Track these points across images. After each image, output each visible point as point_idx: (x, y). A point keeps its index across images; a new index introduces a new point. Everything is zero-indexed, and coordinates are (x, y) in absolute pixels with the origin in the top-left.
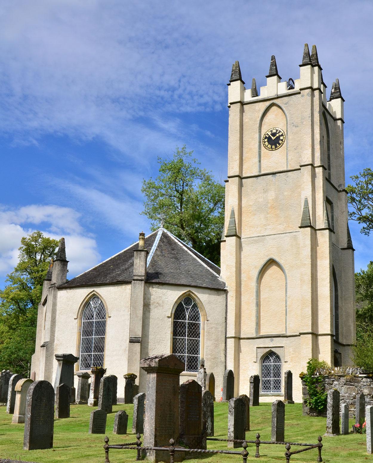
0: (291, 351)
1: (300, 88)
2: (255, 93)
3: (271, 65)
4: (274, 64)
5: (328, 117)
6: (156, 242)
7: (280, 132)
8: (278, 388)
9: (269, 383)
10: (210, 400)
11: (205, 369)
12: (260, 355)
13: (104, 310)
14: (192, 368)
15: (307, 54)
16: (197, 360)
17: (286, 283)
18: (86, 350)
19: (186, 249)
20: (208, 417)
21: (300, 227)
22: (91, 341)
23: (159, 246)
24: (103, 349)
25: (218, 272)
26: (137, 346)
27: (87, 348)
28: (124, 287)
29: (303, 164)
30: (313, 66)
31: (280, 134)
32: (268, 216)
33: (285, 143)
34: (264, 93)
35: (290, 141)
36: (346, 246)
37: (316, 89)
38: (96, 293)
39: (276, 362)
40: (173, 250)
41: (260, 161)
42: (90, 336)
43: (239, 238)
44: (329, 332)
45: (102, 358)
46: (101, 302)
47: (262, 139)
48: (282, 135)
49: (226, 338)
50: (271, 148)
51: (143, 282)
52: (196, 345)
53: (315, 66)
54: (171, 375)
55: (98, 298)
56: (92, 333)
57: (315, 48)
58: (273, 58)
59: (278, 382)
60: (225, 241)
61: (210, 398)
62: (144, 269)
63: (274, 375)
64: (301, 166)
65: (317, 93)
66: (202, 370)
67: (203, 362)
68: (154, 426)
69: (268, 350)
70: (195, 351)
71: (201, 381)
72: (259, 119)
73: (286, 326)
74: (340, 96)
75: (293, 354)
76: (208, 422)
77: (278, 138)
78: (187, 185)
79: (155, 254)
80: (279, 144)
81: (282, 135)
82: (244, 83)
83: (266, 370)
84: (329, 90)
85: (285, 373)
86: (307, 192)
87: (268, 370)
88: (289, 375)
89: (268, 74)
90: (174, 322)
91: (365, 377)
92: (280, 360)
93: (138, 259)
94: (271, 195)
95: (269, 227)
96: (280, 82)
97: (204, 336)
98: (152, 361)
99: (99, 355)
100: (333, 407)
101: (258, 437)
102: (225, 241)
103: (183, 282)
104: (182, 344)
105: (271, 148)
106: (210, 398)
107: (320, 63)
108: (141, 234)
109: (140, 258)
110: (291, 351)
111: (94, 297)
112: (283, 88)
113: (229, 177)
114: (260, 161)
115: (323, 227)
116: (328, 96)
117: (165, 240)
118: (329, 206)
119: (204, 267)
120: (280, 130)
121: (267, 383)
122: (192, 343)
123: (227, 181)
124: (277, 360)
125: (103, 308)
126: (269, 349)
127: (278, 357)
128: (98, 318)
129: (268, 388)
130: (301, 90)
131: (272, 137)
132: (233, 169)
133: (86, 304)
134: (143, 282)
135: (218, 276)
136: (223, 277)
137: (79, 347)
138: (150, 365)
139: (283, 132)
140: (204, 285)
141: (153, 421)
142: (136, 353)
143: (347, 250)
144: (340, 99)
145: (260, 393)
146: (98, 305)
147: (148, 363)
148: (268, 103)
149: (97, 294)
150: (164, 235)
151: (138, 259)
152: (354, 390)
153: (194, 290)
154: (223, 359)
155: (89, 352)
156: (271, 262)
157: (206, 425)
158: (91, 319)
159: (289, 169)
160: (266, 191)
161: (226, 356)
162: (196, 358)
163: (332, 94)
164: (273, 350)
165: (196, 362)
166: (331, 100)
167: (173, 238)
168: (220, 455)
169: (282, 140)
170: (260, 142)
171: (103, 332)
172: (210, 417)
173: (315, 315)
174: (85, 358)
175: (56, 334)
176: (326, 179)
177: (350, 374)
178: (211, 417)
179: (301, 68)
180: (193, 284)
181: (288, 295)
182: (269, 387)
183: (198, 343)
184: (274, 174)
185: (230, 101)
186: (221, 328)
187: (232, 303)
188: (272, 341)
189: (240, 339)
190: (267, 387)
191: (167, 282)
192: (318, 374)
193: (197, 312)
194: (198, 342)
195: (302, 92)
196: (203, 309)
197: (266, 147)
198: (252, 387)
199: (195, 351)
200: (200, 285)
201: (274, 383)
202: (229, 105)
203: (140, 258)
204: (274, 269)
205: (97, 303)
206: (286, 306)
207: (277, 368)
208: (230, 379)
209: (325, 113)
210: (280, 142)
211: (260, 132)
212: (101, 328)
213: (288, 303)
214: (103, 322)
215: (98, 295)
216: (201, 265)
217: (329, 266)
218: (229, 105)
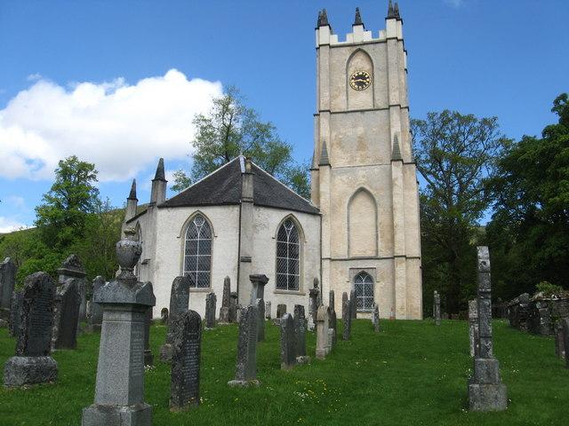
4: (358, 15)
12: (353, 276)
28: (231, 208)
34: (350, 39)
69: (360, 271)
78: (235, 120)
103: (285, 205)
111: (200, 217)
127: (370, 279)
148: (355, 49)
153: (294, 214)
156: (362, 190)
160: (354, 127)
164: (366, 270)
173: (110, 308)
184: (362, 111)
204: (361, 199)
212: (207, 247)
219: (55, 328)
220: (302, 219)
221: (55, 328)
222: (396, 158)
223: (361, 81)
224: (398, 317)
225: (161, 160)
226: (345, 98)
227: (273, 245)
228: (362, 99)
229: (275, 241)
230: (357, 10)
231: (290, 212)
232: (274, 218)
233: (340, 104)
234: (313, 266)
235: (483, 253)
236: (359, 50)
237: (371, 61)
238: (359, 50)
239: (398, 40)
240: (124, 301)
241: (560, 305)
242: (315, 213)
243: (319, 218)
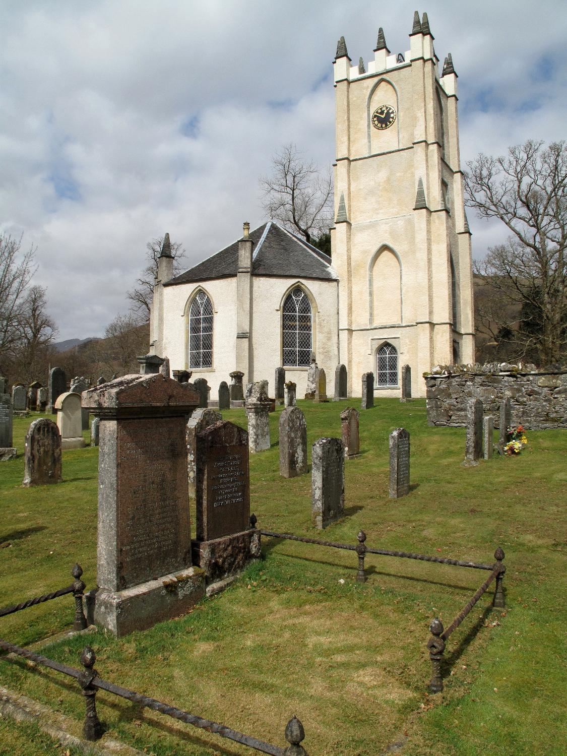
0: (407, 341)
1: (410, 60)
2: (362, 70)
3: (379, 38)
4: (381, 36)
5: (441, 93)
6: (264, 233)
8: (394, 381)
9: (385, 376)
10: (300, 420)
11: (316, 364)
13: (210, 306)
14: (303, 363)
15: (417, 22)
16: (309, 354)
17: (401, 270)
18: (194, 347)
19: (296, 240)
20: (299, 445)
21: (414, 209)
22: (199, 338)
23: (267, 237)
24: (211, 346)
25: (329, 262)
26: (246, 341)
27: (196, 345)
28: (229, 280)
29: (416, 141)
30: (424, 35)
32: (380, 199)
33: (396, 120)
34: (372, 69)
35: (401, 118)
37: (428, 60)
38: (201, 289)
39: (392, 354)
40: (282, 241)
41: (370, 142)
42: (198, 332)
43: (349, 224)
44: (448, 321)
45: (211, 355)
46: (208, 297)
47: (371, 118)
49: (339, 330)
50: (382, 126)
51: (249, 274)
52: (308, 339)
53: (426, 34)
54: (164, 419)
55: (204, 293)
56: (199, 330)
57: (425, 15)
58: (381, 30)
59: (395, 375)
60: (335, 228)
61: (301, 417)
62: (249, 260)
63: (390, 367)
64: (414, 144)
65: (429, 64)
68: (115, 543)
69: (384, 340)
70: (306, 345)
71: (313, 376)
72: (367, 97)
73: (402, 316)
74: (453, 72)
75: (409, 345)
76: (297, 452)
77: (388, 114)
79: (263, 246)
80: (390, 122)
82: (350, 60)
83: (382, 365)
84: (441, 66)
85: (403, 368)
87: (384, 362)
88: (408, 370)
89: (376, 48)
90: (284, 315)
91: (507, 376)
92: (396, 351)
93: (243, 251)
94: (383, 175)
95: (381, 211)
96: (389, 56)
97: (315, 329)
98: (103, 395)
99: (207, 353)
100: (475, 424)
101: (363, 539)
102: (335, 228)
103: (294, 273)
104: (293, 338)
105: (382, 126)
106: (301, 417)
107: (431, 32)
108: (245, 224)
109: (245, 248)
110: (407, 341)
111: (201, 292)
112: (391, 62)
113: (337, 160)
114: (370, 142)
115: (440, 209)
116: (441, 72)
118: (444, 188)
119: (315, 257)
120: (391, 107)
121: (383, 376)
122: (303, 337)
123: (335, 165)
124: (393, 352)
125: (209, 304)
126: (386, 340)
127: (394, 350)
128: (205, 315)
129: (384, 381)
130: (412, 61)
131: (382, 116)
133: (193, 301)
134: (249, 274)
135: (328, 265)
136: (334, 266)
137: (187, 346)
138: (100, 404)
139: (393, 109)
140: (314, 275)
141: (114, 532)
142: (244, 350)
144: (453, 74)
145: (374, 387)
146: (205, 300)
147: (97, 398)
148: (376, 79)
149: (203, 289)
151: (243, 251)
152: (493, 393)
154: (336, 353)
155: (198, 349)
156: (385, 248)
157: (295, 456)
158: (198, 315)
159: (401, 148)
161: (339, 349)
162: (308, 352)
163: (444, 70)
164: (388, 341)
165: (308, 356)
166: (443, 75)
169: (393, 118)
172: (300, 445)
174: (194, 356)
175: (165, 332)
176: (441, 159)
177: (543, 394)
178: (302, 444)
179: (412, 37)
180: (303, 275)
181: (403, 283)
182: (385, 380)
183: (309, 337)
185: (337, 79)
187: (344, 293)
189: (353, 331)
190: (383, 380)
191: (275, 273)
192: (446, 373)
193: (308, 304)
194: (309, 336)
195: (413, 63)
197: (375, 126)
198: (365, 386)
199: (306, 345)
200: (310, 276)
201: (390, 376)
202: (335, 84)
203: (245, 248)
204: (386, 253)
205: (203, 298)
206: (401, 295)
207: (393, 360)
208: (342, 374)
209: (439, 90)
210: (391, 120)
211: (369, 110)
213: (403, 291)
214: (210, 318)
215: (204, 290)
216: (311, 255)
217: (446, 250)
218: (335, 84)
219: (191, 457)
220: (312, 287)
221: (191, 457)
222: (421, 205)
223: (383, 120)
224: (374, 391)
225: (343, 38)
226: (366, 141)
227: (278, 317)
228: (387, 139)
231: (297, 280)
232: (276, 289)
233: (360, 149)
234: (329, 339)
236: (383, 80)
239: (425, 61)
241: (451, 383)
243: (335, 283)
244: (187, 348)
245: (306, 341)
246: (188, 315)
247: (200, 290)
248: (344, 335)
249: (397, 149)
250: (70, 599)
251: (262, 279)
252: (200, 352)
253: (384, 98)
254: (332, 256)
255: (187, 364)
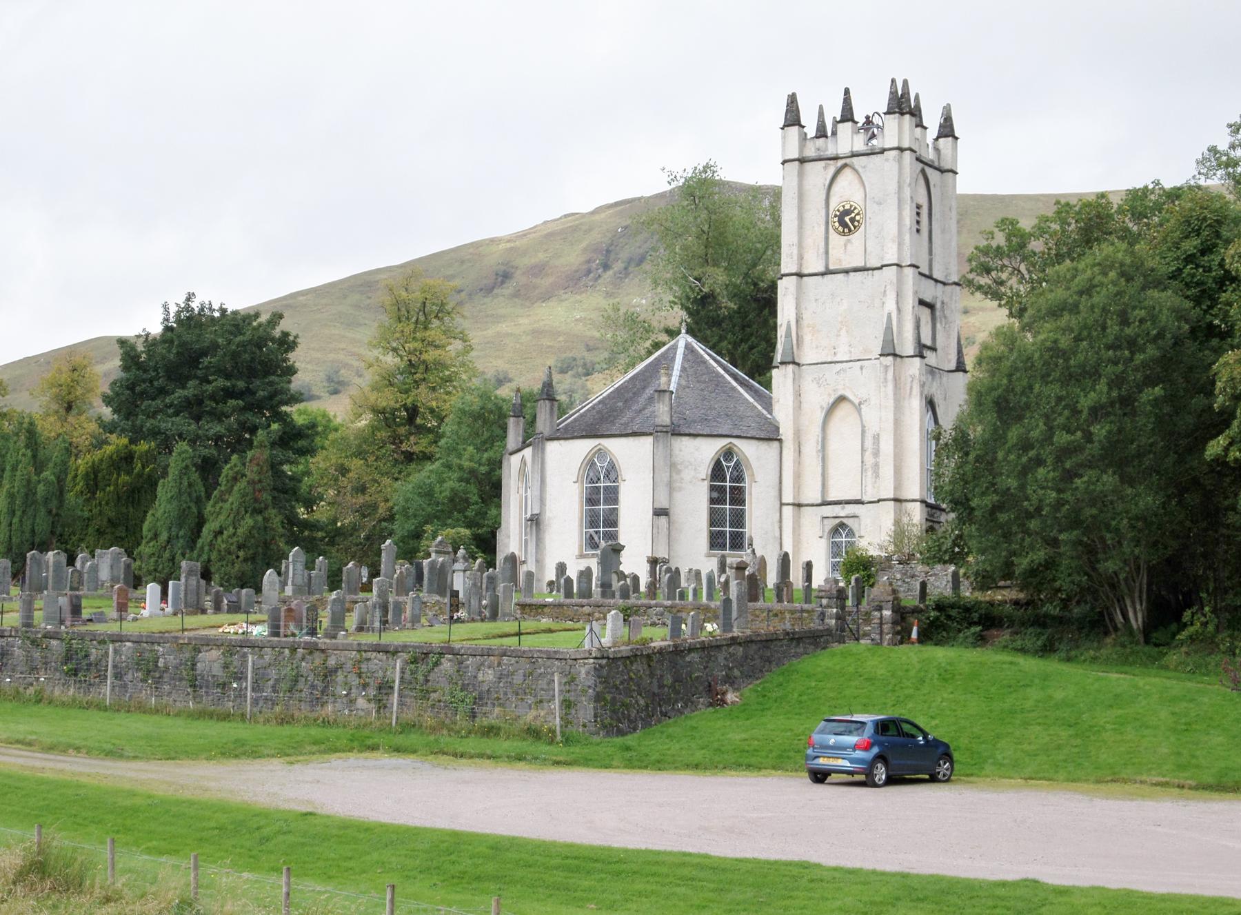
7: (855, 208)
12: (827, 529)
15: (893, 93)
23: (683, 369)
26: (663, 519)
31: (856, 211)
33: (863, 226)
36: (953, 366)
48: (858, 214)
57: (905, 82)
66: (749, 551)
67: (751, 539)
69: (837, 521)
81: (858, 214)
86: (891, 306)
111: (600, 452)
117: (690, 357)
127: (851, 533)
132: (787, 265)
143: (957, 373)
148: (840, 163)
150: (688, 347)
153: (735, 441)
164: (845, 521)
167: (702, 352)
168: (571, 300)
169: (858, 221)
170: (827, 223)
171: (615, 500)
180: (736, 432)
186: (775, 493)
188: (843, 508)
196: (749, 467)
197: (836, 230)
220: (749, 450)
223: (846, 221)
229: (706, 482)
230: (847, 92)
231: (724, 442)
235: (49, 627)
237: (860, 177)
238: (845, 165)
240: (163, 859)
242: (771, 435)
243: (776, 444)
244: (581, 526)
245: (738, 519)
246: (582, 483)
247: (600, 449)
248: (788, 511)
249: (861, 264)
250: (785, 508)
251: (685, 439)
252: (724, 533)
253: (847, 191)
254: (774, 391)
255: (581, 546)
